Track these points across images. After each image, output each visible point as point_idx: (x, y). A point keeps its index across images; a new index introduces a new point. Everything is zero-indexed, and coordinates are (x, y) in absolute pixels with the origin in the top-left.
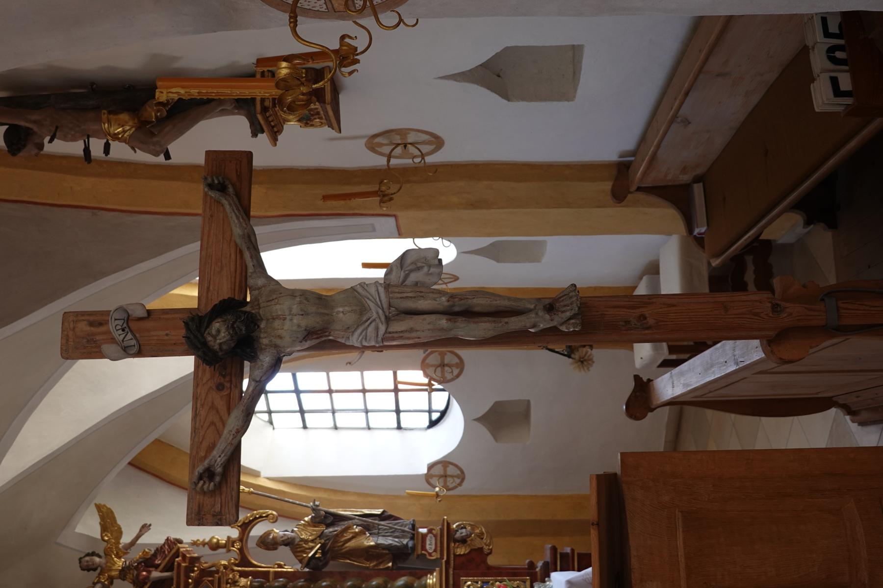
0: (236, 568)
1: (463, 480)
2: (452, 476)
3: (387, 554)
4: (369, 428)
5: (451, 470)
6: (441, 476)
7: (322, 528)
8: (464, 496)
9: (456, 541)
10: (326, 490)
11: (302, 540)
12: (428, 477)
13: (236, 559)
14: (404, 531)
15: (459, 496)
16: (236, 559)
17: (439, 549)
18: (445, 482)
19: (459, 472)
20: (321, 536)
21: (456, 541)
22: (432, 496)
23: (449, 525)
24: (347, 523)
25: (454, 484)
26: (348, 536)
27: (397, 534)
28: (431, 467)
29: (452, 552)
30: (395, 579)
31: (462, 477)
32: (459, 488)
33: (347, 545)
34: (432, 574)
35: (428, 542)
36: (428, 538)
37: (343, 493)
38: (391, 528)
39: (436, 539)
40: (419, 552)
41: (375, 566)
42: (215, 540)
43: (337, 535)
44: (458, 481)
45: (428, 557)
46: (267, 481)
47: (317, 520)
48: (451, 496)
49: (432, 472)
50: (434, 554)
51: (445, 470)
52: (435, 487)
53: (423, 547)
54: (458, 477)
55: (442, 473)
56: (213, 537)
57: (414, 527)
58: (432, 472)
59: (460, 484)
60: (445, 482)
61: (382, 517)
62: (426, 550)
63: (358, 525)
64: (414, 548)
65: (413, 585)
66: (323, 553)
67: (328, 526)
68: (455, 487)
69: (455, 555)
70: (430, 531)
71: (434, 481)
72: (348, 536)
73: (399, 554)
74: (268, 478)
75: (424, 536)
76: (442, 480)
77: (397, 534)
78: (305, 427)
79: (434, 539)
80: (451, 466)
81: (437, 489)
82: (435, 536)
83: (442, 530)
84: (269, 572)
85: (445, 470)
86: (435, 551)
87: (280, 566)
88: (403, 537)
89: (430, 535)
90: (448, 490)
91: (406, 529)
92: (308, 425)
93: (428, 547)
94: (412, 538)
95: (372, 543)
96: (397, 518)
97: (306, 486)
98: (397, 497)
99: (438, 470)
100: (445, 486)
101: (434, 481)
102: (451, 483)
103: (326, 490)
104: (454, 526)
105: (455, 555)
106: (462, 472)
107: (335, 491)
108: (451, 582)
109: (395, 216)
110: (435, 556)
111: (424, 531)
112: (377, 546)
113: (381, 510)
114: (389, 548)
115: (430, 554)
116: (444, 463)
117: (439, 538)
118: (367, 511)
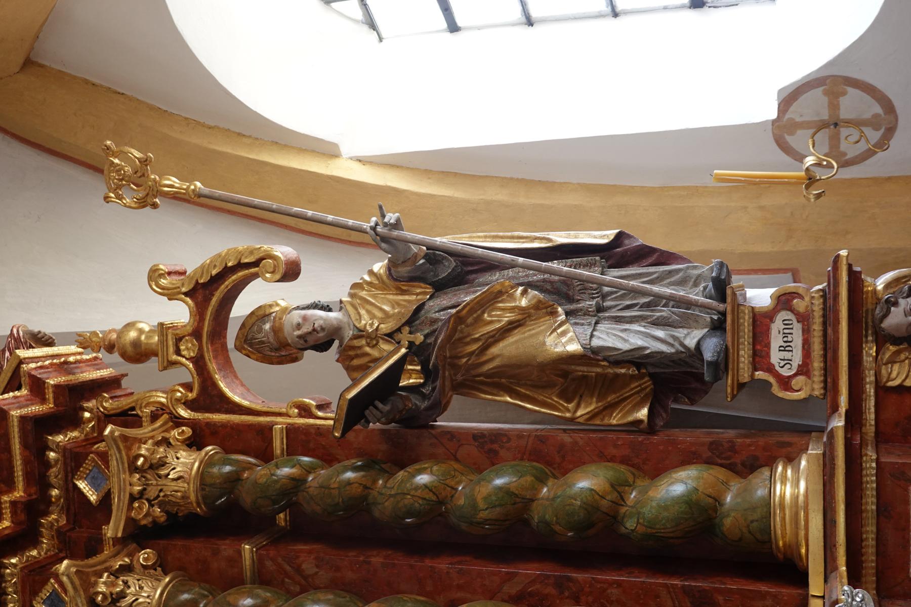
0: (183, 413)
1: (891, 131)
2: (857, 124)
3: (633, 378)
4: (615, 15)
5: (854, 104)
6: (822, 126)
7: (418, 294)
8: (889, 179)
9: (883, 339)
10: (505, 182)
11: (361, 333)
12: (782, 130)
13: (188, 387)
14: (689, 304)
15: (876, 181)
16: (188, 387)
17: (817, 364)
18: (835, 141)
19: (878, 109)
20: (413, 320)
21: (883, 339)
22: (797, 182)
23: (855, 279)
24: (496, 277)
25: (863, 146)
26: (498, 317)
27: (663, 312)
28: (790, 98)
29: (870, 378)
30: (657, 470)
31: (887, 121)
32: (880, 155)
33: (494, 350)
34: (791, 459)
35: (776, 341)
36: (777, 326)
37: (549, 186)
38: (644, 293)
39: (806, 331)
40: (745, 377)
41: (593, 415)
42: (133, 334)
43: (459, 319)
44: (874, 136)
45: (776, 390)
46: (357, 166)
47: (404, 270)
48: (852, 182)
49: (794, 113)
50: (799, 381)
51: (834, 107)
52: (800, 158)
53: (760, 358)
54: (874, 122)
55: (825, 116)
56: (130, 326)
57: (721, 287)
58: (794, 113)
59: (882, 144)
60: (835, 141)
61: (617, 253)
62: (770, 369)
63: (529, 285)
64: (722, 365)
65: (718, 501)
66: (428, 373)
67: (440, 287)
68: (869, 154)
69: (882, 390)
70: (784, 301)
71: (800, 140)
72: (498, 317)
73: (672, 381)
74: (360, 160)
75: (761, 321)
76: (823, 136)
77: (663, 312)
78: (453, 28)
79: (797, 329)
80: (851, 90)
81: (810, 161)
82: (804, 319)
83: (829, 298)
84: (269, 428)
85: (834, 107)
86: (804, 370)
87: (304, 411)
88: (686, 322)
89: (784, 315)
90: (845, 164)
91: (696, 295)
92: (460, 23)
93: (775, 357)
94: (718, 327)
95: (574, 347)
96: (665, 258)
97: (456, 174)
98: (695, 191)
99: (814, 106)
100: (834, 151)
101: (800, 140)
102: (850, 145)
103: (505, 182)
104: (880, 283)
105: (882, 390)
106: (889, 107)
107: (528, 184)
108: (870, 504)
109: (825, 395)
110: (805, 389)
111: (760, 296)
112: (591, 356)
113: (611, 234)
114: (637, 360)
115: (785, 383)
116: (831, 82)
117: (817, 327)
118: (561, 238)
